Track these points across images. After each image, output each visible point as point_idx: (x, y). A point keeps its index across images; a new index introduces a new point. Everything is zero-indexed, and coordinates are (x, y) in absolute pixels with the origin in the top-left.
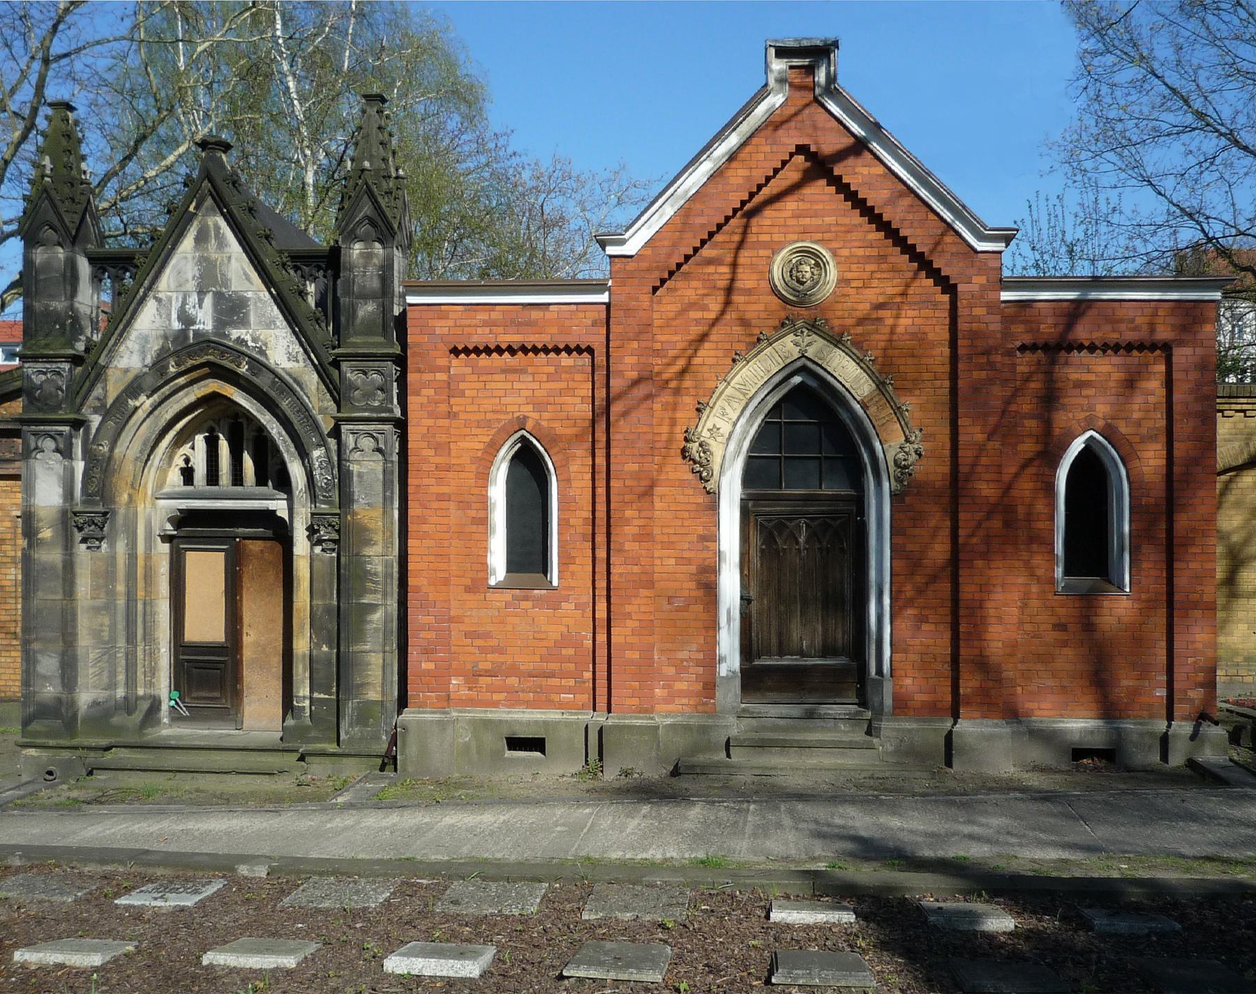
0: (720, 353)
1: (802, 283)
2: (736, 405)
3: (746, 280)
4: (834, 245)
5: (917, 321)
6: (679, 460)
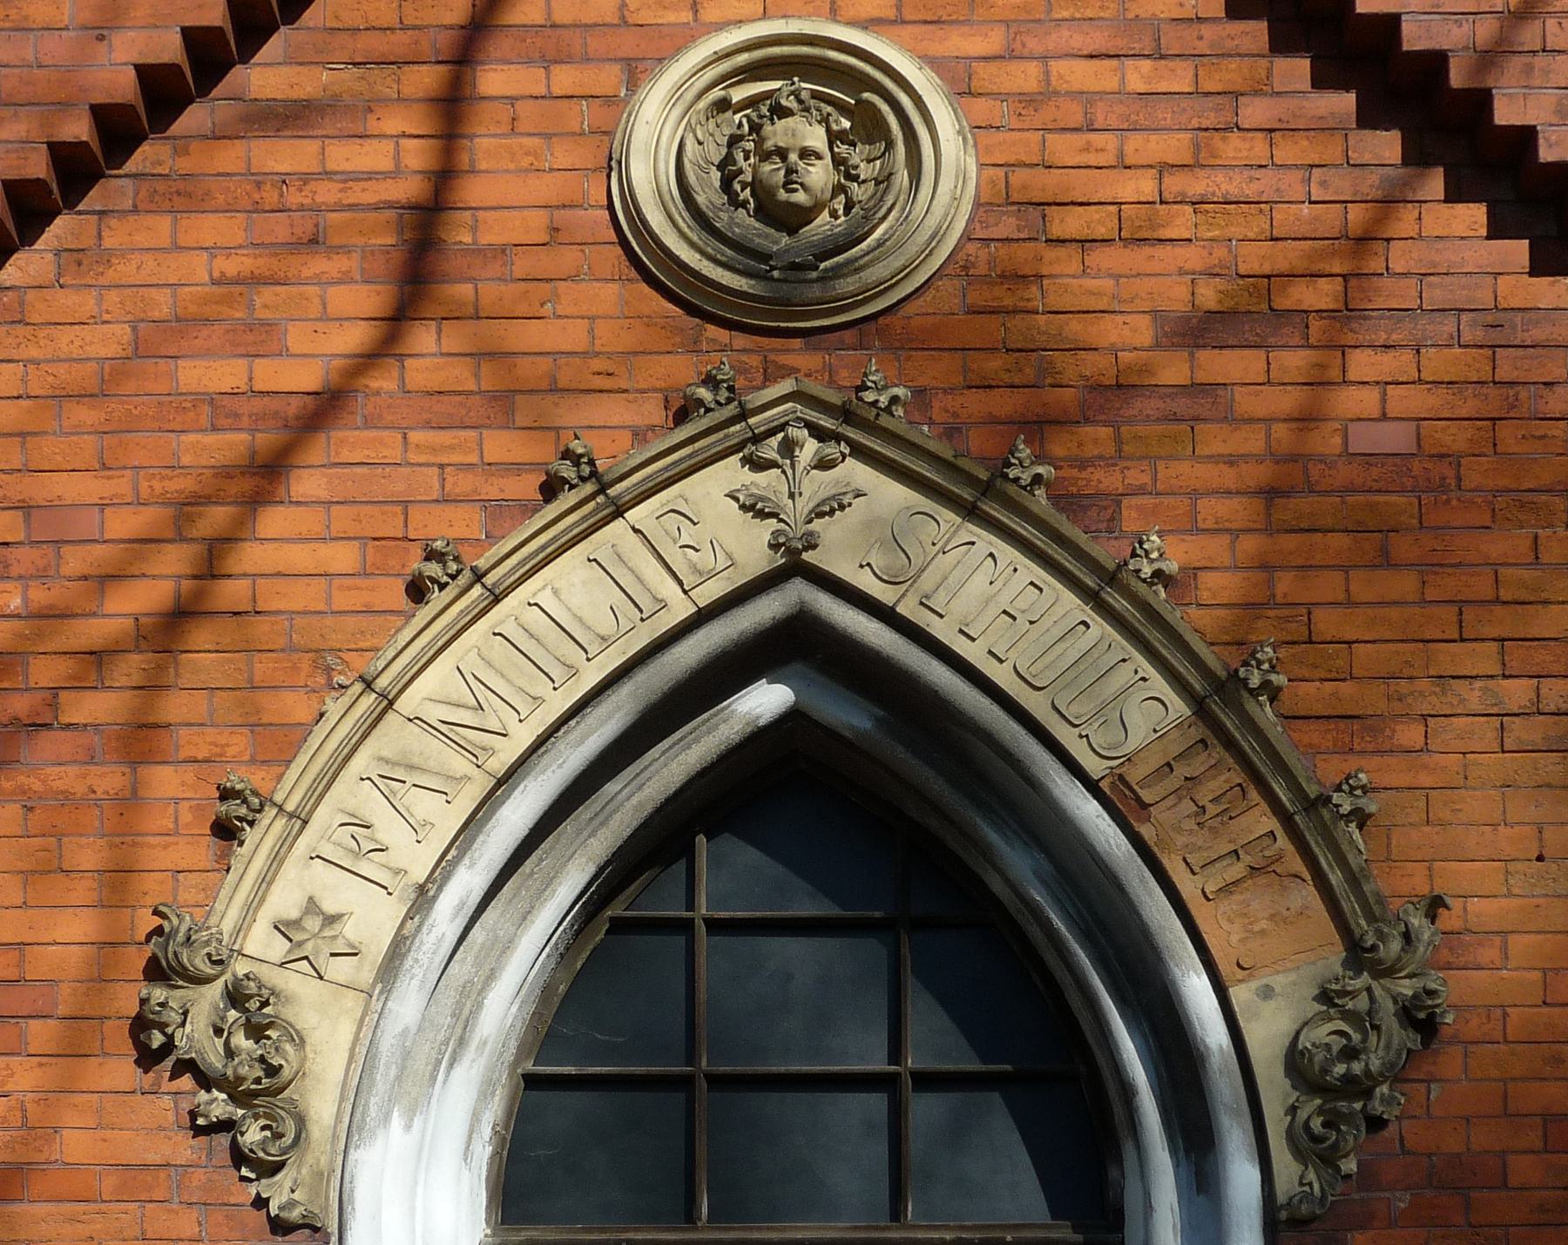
0: (343, 557)
1: (791, 219)
2: (424, 805)
3: (507, 191)
4: (961, 43)
5: (1406, 401)
6: (122, 1070)
